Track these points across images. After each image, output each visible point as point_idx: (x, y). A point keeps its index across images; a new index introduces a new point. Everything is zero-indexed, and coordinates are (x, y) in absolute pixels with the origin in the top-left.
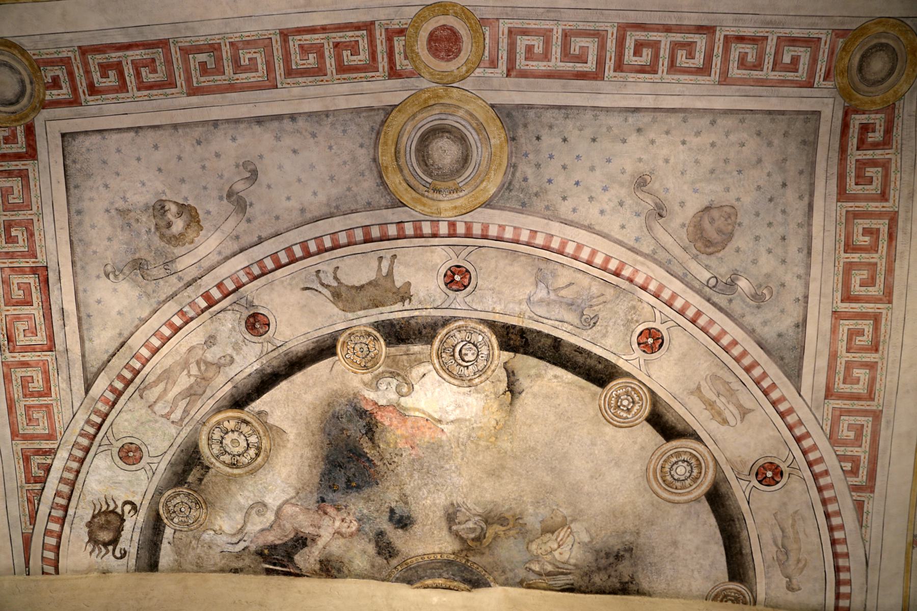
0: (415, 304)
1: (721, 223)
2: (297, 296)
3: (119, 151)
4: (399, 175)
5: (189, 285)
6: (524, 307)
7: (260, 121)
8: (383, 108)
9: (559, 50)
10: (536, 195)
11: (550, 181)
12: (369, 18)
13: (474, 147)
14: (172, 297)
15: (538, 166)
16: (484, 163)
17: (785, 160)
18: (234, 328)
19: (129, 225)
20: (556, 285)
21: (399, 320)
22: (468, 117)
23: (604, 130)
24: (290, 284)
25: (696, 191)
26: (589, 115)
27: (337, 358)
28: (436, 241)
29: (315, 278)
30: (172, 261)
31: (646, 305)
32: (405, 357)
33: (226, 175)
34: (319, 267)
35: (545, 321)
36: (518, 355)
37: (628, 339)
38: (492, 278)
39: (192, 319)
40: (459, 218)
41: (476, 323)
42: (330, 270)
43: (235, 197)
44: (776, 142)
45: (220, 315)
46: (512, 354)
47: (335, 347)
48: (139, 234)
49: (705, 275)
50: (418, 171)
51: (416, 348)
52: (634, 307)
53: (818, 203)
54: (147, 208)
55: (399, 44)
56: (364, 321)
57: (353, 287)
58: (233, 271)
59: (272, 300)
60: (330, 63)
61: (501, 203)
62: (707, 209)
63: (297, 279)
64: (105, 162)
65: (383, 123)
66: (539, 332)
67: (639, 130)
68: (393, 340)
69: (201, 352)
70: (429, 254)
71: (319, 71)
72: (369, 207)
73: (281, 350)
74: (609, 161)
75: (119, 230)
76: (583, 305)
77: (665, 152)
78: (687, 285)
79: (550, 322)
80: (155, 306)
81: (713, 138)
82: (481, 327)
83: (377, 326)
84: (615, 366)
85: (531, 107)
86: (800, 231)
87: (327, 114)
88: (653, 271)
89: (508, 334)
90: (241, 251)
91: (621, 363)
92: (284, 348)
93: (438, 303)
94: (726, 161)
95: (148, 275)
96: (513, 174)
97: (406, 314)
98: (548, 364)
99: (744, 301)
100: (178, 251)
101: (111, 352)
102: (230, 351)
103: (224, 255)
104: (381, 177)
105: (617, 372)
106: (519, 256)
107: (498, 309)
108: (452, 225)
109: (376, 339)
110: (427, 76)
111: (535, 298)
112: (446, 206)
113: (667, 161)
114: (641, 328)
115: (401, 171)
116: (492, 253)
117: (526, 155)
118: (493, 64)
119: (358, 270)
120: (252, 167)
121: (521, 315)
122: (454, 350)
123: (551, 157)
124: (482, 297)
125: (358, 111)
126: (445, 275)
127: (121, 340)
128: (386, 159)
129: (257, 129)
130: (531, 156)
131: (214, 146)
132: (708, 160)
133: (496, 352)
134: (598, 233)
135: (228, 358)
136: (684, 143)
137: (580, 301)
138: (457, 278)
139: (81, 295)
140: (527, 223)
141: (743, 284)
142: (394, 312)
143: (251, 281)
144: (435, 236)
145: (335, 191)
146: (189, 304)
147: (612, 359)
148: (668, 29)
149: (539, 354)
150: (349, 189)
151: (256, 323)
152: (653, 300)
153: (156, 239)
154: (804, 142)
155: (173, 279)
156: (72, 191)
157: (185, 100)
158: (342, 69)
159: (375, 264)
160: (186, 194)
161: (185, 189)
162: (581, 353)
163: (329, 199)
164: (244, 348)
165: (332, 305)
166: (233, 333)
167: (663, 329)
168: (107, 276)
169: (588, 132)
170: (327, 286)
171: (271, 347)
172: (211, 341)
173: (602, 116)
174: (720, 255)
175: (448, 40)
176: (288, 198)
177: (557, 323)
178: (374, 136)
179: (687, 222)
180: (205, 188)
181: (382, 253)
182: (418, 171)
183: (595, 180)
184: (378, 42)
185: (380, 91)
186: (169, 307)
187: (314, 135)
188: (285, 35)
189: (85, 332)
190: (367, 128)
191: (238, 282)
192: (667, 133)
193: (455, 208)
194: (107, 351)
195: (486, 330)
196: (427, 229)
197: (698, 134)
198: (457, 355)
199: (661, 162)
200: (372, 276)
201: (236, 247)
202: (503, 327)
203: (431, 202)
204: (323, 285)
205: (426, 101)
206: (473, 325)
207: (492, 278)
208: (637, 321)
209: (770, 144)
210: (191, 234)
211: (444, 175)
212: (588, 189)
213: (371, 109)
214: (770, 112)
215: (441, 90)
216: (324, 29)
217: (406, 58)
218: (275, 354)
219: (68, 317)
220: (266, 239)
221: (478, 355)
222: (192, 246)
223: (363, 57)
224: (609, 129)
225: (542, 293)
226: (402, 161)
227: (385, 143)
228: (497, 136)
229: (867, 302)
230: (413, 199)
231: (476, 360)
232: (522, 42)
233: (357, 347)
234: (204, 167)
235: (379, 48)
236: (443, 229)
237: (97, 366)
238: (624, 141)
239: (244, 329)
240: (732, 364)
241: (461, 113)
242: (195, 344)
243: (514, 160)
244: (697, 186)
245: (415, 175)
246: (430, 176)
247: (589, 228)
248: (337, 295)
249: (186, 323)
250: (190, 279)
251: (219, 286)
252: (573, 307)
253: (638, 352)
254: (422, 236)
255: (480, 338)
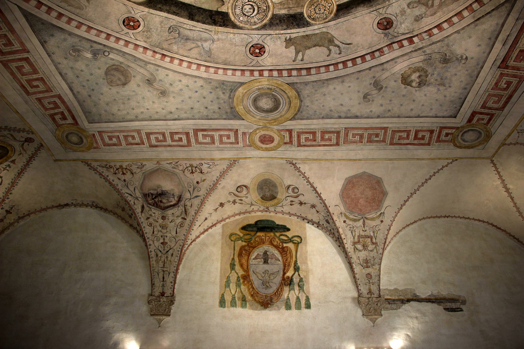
0: (283, 37)
1: (115, 79)
2: (357, 40)
3: (431, 109)
4: (289, 95)
5: (420, 49)
6: (216, 37)
7: (357, 117)
8: (295, 119)
9: (215, 138)
10: (217, 88)
11: (211, 93)
12: (299, 148)
13: (251, 105)
14: (433, 43)
15: (218, 98)
16: (245, 99)
17: (95, 105)
18: (401, 24)
19: (442, 79)
20: (198, 49)
21: (294, 28)
22: (254, 116)
23: (188, 112)
24: (358, 47)
25: (134, 91)
26: (197, 117)
27: (337, 3)
28: (270, 68)
29: (343, 50)
30: (425, 60)
31: (141, 40)
32: (291, 6)
33: (380, 97)
34: (339, 56)
35: (201, 30)
36: (215, 9)
37: (146, 22)
38: (237, 52)
39: (426, 32)
40: (257, 78)
41: (245, 27)
42: (332, 55)
43: (378, 87)
44: (103, 112)
45: (407, 32)
46: (220, 10)
47: (338, 10)
48: (439, 74)
49: (111, 56)
50: (279, 97)
51: (283, 12)
52: (148, 38)
53: (68, 92)
54: (428, 85)
55: (287, 139)
56: (316, 27)
57: (320, 46)
58: (391, 53)
59: (372, 37)
60: (318, 135)
61: (236, 84)
62: (124, 84)
63: (353, 49)
64: (441, 105)
65: (296, 114)
66: (204, 23)
67: (171, 113)
68: (298, 16)
69: (427, 13)
70: (274, 62)
71: (323, 133)
72: (306, 84)
73: (374, 8)
74: (182, 101)
75: (448, 78)
76: (180, 39)
77: (156, 106)
78: (121, 51)
79: (198, 29)
80: (446, 40)
81: (134, 111)
82: (241, 25)
83: (308, 24)
84: (150, 7)
85: (225, 119)
86: (71, 81)
87: (323, 118)
88: (144, 57)
89: (224, 22)
90: (383, 64)
91: (147, 10)
92: (372, 9)
93: (268, 38)
94: (124, 103)
95: (443, 55)
96: (230, 95)
97: (289, 31)
98: (194, 5)
99: (84, 48)
100: (421, 64)
101: (488, 16)
102: (408, 11)
103: (394, 61)
104: (299, 95)
105: (147, 5)
106: (222, 62)
107: (232, 35)
108: (261, 75)
109: (309, 17)
110: (274, 130)
111: (210, 42)
112: (265, 82)
113: (153, 102)
114: (141, 28)
115: (288, 97)
116: (237, 63)
117: (225, 102)
118: (244, 134)
119: (316, 55)
120: (365, 100)
121: (217, 33)
122: (258, 11)
123: (212, 101)
124: (242, 41)
125: (308, 119)
126: (265, 52)
127: (477, 22)
128: (296, 102)
129: (358, 114)
130: (222, 101)
131: (382, 109)
132: (133, 104)
133: (230, 11)
134: (180, 73)
135: (411, 7)
136: (148, 109)
137: (182, 41)
138: (257, 51)
139: (488, 51)
140: (220, 76)
141: (89, 55)
142: (296, 32)
143: (382, 48)
144: (271, 70)
145: (324, 90)
146: (424, 39)
147: (152, 11)
148: (170, 146)
149: (201, 11)
150: (316, 91)
151: (386, 25)
152: (138, 43)
153: (430, 70)
154: (90, 113)
155: (428, 52)
156: (463, 97)
157: (390, 126)
158: (314, 133)
159: (305, 58)
160: (404, 90)
161: (404, 92)
162: (174, 12)
163: (327, 87)
164: (398, 12)
165: (335, 36)
166: (402, 21)
167: (126, 30)
168: (467, 58)
169: (195, 111)
170: (336, 46)
171: (380, 11)
172: (418, 19)
173: (190, 116)
174: (108, 66)
175: (265, 141)
176: (349, 87)
177: (194, 28)
178: (301, 110)
179: (133, 78)
180: (393, 92)
181: (301, 62)
182: (279, 97)
183: (187, 93)
184: (296, 141)
185: (297, 125)
186: (437, 38)
187: (331, 111)
188: (337, 144)
189: (498, 29)
190: (304, 113)
191: (390, 47)
192: (157, 112)
193: (260, 82)
194: (491, 16)
195: (238, 23)
196: (275, 74)
197: (142, 113)
198: (256, 8)
199: (156, 101)
200: (308, 52)
201: (385, 66)
202: (227, 26)
203: (273, 84)
204: (339, 47)
205: (275, 122)
206: (247, 26)
207: (237, 52)
208: (144, 32)
209: (106, 111)
210: (409, 72)
211: (265, 95)
212: (190, 90)
213: (301, 119)
214: (112, 122)
215: (268, 125)
216: (320, 146)
217: (284, 136)
218: (378, 7)
219: (503, 40)
220: (367, 69)
221: (242, 8)
222: (410, 66)
223: (303, 137)
224: (186, 113)
225: (206, 45)
226: (288, 100)
227: (295, 107)
228: (240, 109)
229: (14, 59)
230: (282, 86)
231: (243, 6)
232: (232, 140)
233: (322, 11)
234: (391, 101)
235: (296, 139)
236: (266, 74)
237: (504, 7)
238: (177, 109)
239: (395, 23)
240: (73, 16)
241: (258, 117)
242: (430, 18)
243: (231, 100)
244: (134, 93)
245: (281, 95)
246: (273, 94)
247: (186, 75)
248: (331, 41)
249: (430, 29)
250: (419, 51)
251: (402, 46)
252: (185, 38)
253: (137, 17)
254: (278, 70)
255: (241, 19)
